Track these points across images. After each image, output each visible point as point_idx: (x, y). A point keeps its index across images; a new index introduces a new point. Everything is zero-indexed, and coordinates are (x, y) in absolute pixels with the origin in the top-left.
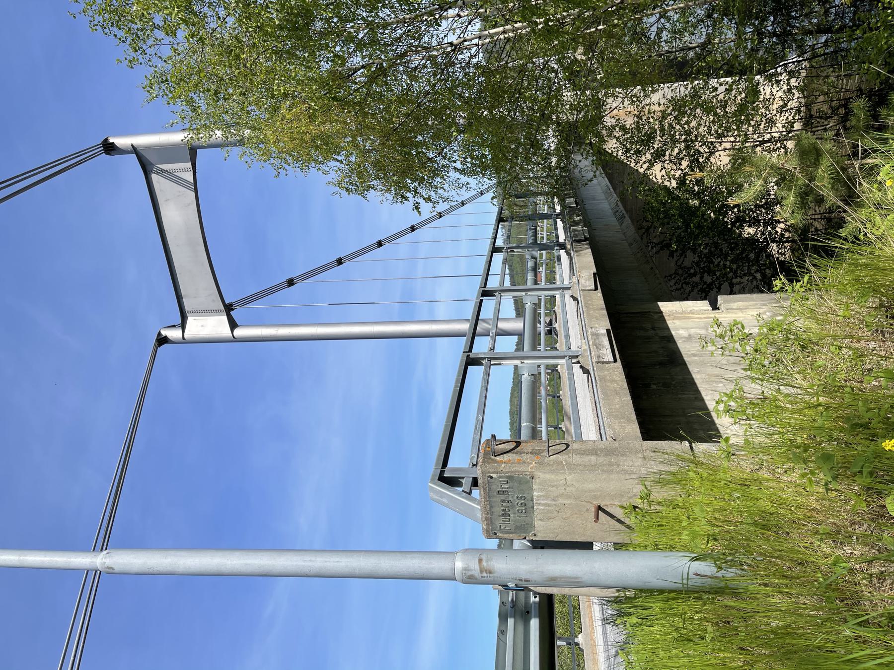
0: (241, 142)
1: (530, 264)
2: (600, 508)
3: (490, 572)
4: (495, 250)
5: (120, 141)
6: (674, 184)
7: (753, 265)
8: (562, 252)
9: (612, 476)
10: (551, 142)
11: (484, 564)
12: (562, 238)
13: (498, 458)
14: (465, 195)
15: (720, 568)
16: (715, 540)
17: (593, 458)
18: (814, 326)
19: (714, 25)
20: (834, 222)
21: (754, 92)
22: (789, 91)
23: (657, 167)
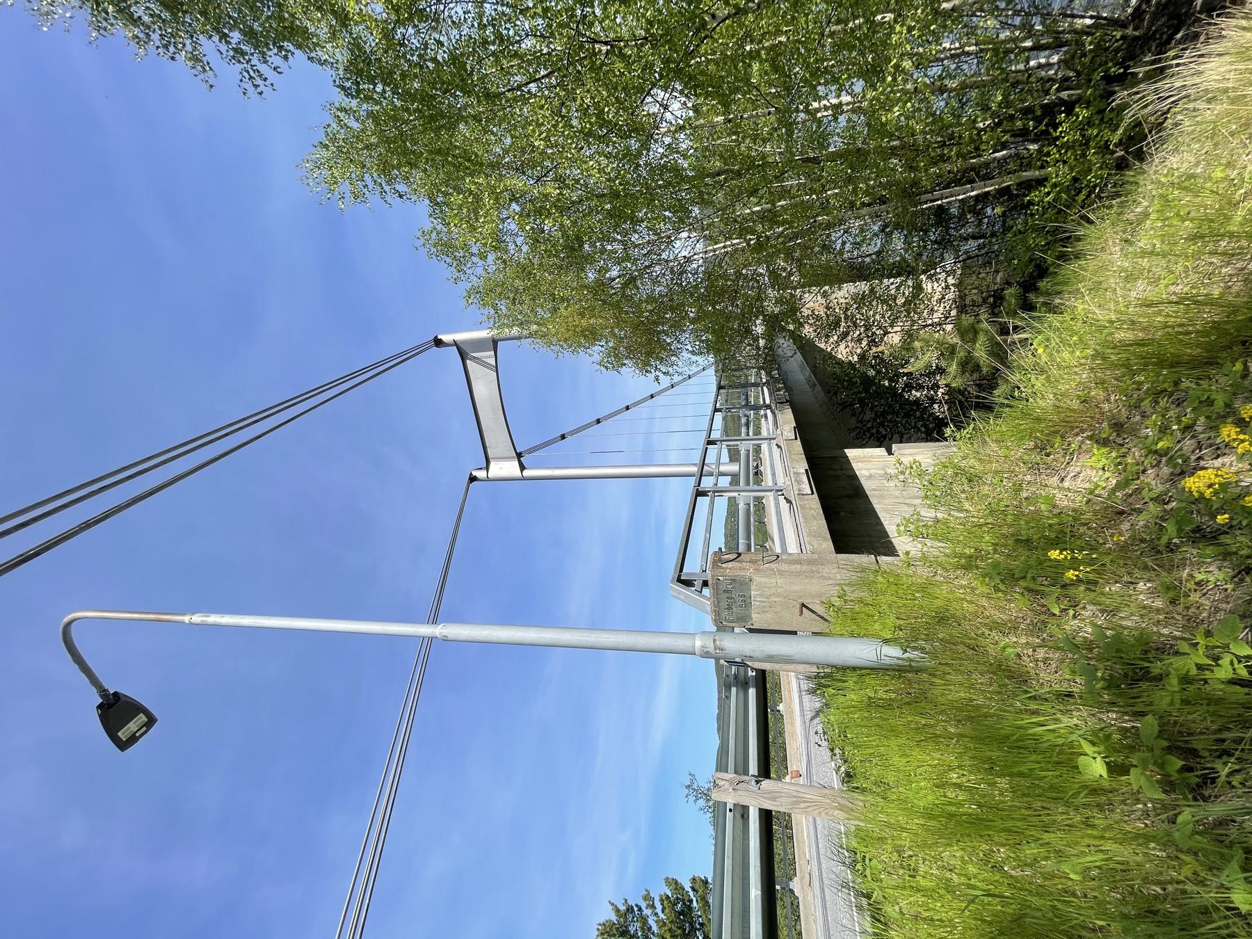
0: (530, 335)
1: (743, 420)
2: (803, 605)
3: (722, 650)
4: (716, 410)
5: (446, 338)
6: (856, 358)
7: (919, 421)
8: (769, 411)
9: (814, 581)
10: (759, 329)
11: (718, 643)
12: (768, 402)
13: (723, 565)
14: (694, 369)
15: (906, 651)
16: (901, 630)
17: (798, 567)
18: (977, 464)
19: (886, 237)
20: (989, 382)
21: (918, 288)
22: (947, 287)
23: (842, 346)
